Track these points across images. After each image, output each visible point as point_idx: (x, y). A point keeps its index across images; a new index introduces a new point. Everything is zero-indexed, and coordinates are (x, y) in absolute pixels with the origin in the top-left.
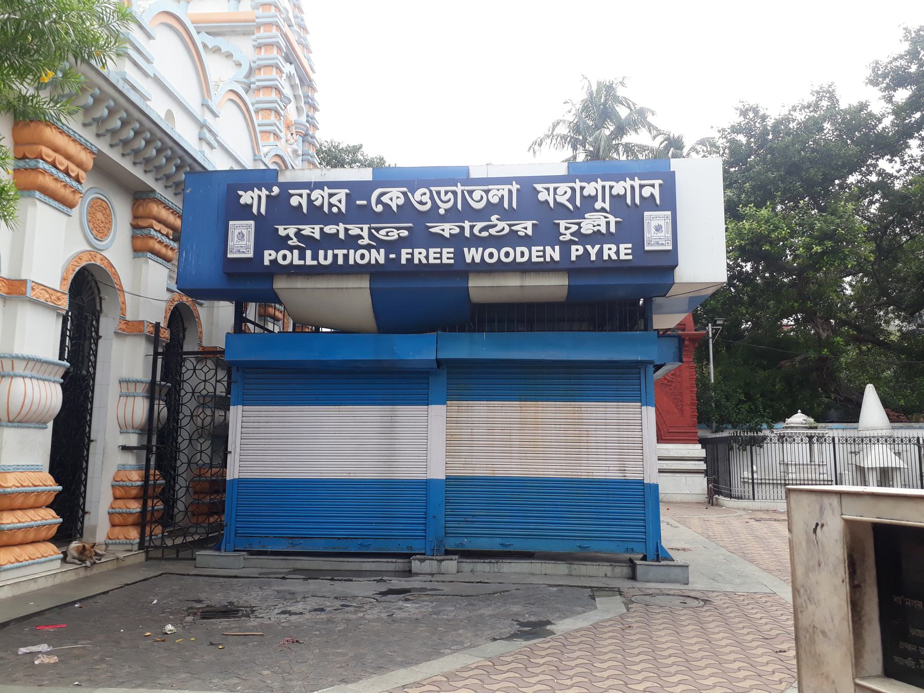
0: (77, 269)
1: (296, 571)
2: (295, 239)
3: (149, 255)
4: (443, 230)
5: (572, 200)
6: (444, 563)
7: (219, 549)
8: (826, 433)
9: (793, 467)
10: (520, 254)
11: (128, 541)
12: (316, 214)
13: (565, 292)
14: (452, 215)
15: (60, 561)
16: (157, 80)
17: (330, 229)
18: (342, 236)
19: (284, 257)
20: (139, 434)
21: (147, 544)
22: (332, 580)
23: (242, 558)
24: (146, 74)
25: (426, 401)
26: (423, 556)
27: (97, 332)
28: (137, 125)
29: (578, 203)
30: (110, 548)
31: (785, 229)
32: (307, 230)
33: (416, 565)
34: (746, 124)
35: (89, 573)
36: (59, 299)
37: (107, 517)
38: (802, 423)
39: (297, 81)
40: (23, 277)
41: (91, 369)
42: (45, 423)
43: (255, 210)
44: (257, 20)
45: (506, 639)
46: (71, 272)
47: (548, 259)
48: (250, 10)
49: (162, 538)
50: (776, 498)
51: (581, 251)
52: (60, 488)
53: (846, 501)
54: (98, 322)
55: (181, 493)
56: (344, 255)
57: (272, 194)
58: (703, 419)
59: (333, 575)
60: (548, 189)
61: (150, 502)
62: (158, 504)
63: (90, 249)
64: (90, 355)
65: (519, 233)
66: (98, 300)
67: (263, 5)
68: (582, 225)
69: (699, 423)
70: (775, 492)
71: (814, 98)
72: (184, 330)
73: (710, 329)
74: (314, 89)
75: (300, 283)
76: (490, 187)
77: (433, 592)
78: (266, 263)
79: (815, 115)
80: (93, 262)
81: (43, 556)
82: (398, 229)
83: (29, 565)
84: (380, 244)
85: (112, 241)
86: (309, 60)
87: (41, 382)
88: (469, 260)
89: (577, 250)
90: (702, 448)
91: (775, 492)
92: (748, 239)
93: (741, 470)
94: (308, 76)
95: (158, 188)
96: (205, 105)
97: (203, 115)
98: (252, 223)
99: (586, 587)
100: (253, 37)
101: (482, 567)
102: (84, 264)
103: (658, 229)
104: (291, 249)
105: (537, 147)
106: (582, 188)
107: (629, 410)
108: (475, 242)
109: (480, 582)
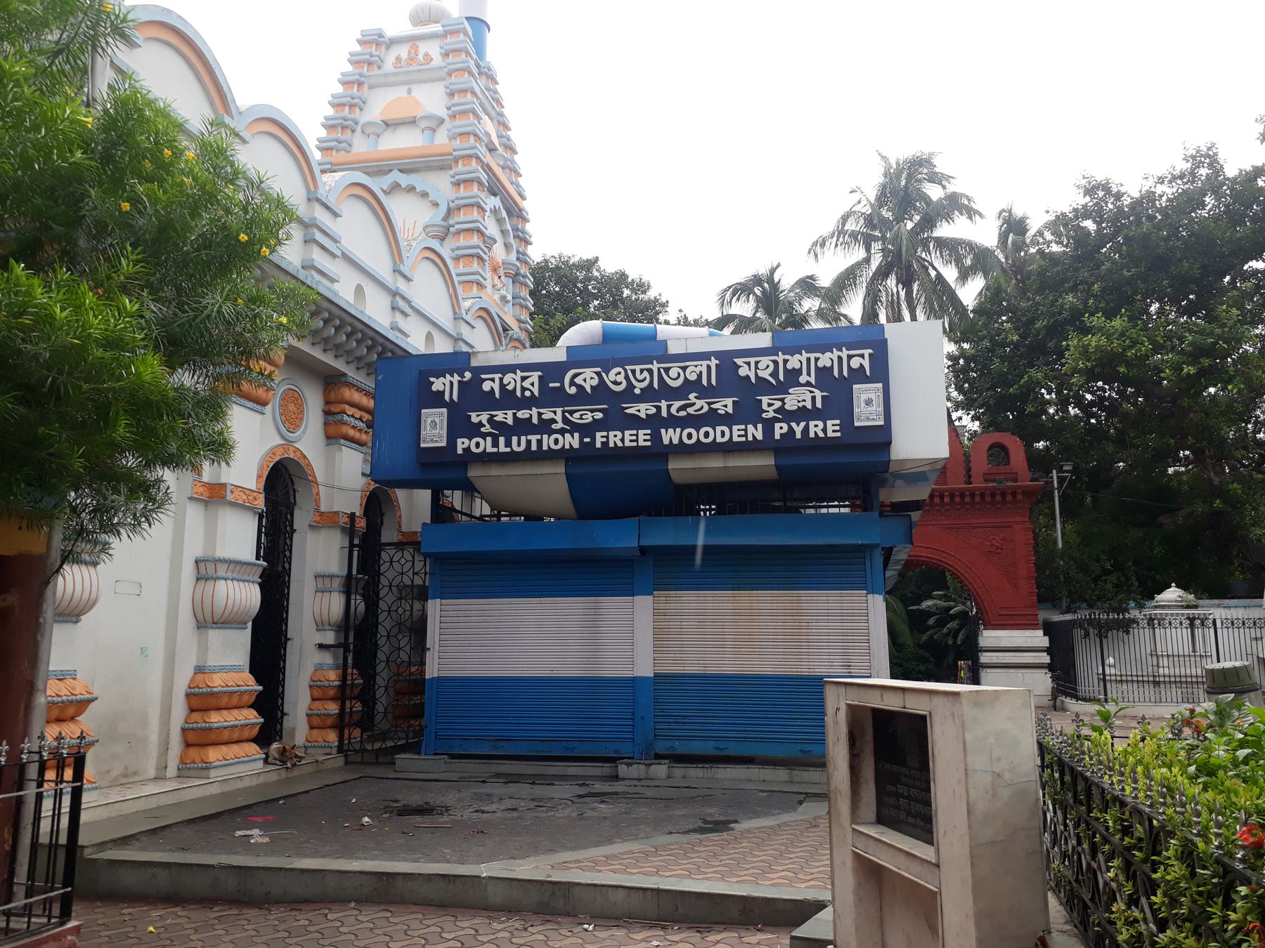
0: (271, 465)
1: (498, 775)
2: (488, 426)
3: (342, 441)
4: (639, 411)
5: (775, 374)
6: (653, 767)
7: (419, 753)
8: (1210, 614)
9: (1165, 659)
10: (719, 434)
11: (327, 744)
12: (509, 399)
13: (773, 474)
14: (649, 395)
15: (262, 761)
16: (347, 258)
17: (523, 414)
18: (535, 421)
19: (478, 445)
20: (336, 631)
21: (346, 748)
22: (533, 783)
23: (442, 761)
24: (334, 256)
25: (630, 591)
26: (631, 760)
27: (292, 525)
28: (327, 315)
29: (781, 377)
30: (310, 751)
31: (1146, 344)
32: (500, 416)
33: (623, 770)
34: (1094, 204)
35: (290, 775)
36: (255, 499)
37: (305, 719)
38: (1176, 601)
39: (504, 214)
40: (223, 481)
41: (287, 565)
42: (246, 623)
43: (447, 397)
44: (455, 153)
45: (683, 833)
46: (266, 468)
47: (750, 438)
48: (446, 141)
49: (361, 742)
50: (1137, 700)
51: (785, 429)
52: (261, 688)
53: (849, 688)
54: (292, 516)
55: (380, 692)
56: (538, 440)
57: (464, 380)
58: (1047, 598)
59: (534, 780)
60: (748, 364)
61: (348, 703)
62: (356, 705)
63: (283, 442)
64: (285, 551)
65: (719, 411)
66: (292, 493)
67: (461, 134)
68: (785, 401)
69: (1039, 601)
70: (1141, 692)
71: (1189, 165)
72: (382, 515)
73: (1055, 478)
74: (526, 220)
75: (494, 471)
76: (687, 363)
77: (635, 796)
78: (460, 451)
79: (1191, 187)
80: (286, 456)
81: (247, 756)
82: (592, 411)
83: (235, 763)
84: (573, 428)
85: (304, 432)
86: (518, 185)
87: (241, 583)
88: (666, 441)
89: (781, 428)
90: (1045, 635)
91: (1141, 692)
92: (1096, 360)
93: (1088, 666)
94: (515, 203)
95: (350, 372)
96: (397, 271)
97: (395, 282)
98: (444, 410)
99: (801, 793)
100: (451, 172)
101: (695, 773)
102: (277, 458)
103: (869, 402)
104: (484, 436)
105: (818, 249)
106: (786, 361)
107: (852, 599)
108: (673, 422)
109: (688, 787)
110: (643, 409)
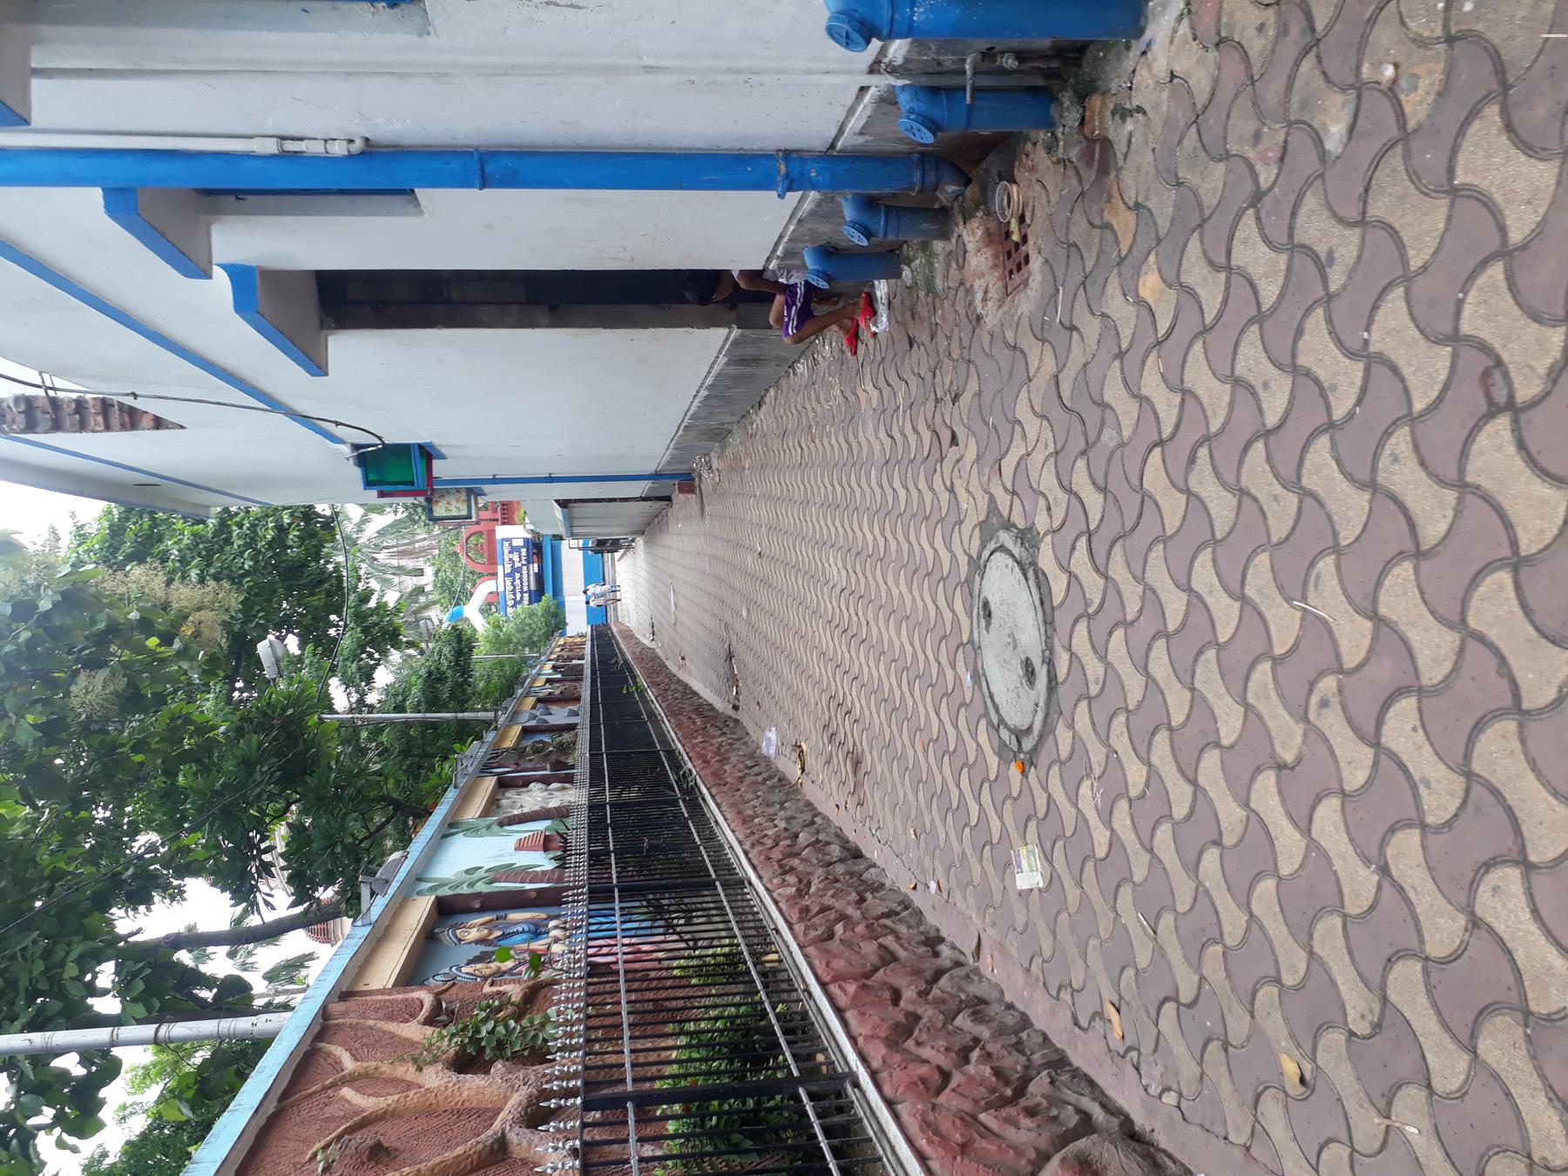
10: (525, 576)
14: (515, 594)
110: (519, 596)
